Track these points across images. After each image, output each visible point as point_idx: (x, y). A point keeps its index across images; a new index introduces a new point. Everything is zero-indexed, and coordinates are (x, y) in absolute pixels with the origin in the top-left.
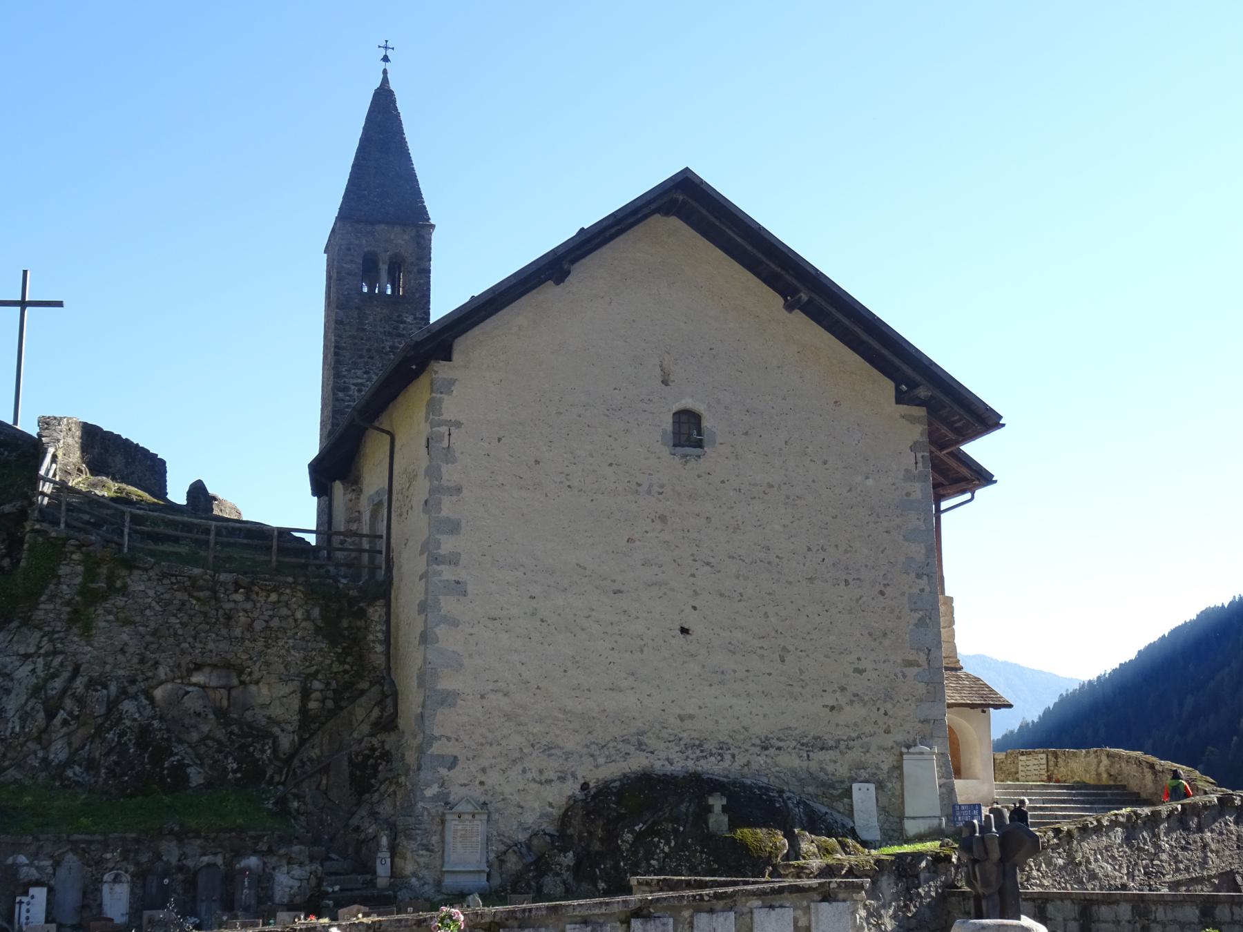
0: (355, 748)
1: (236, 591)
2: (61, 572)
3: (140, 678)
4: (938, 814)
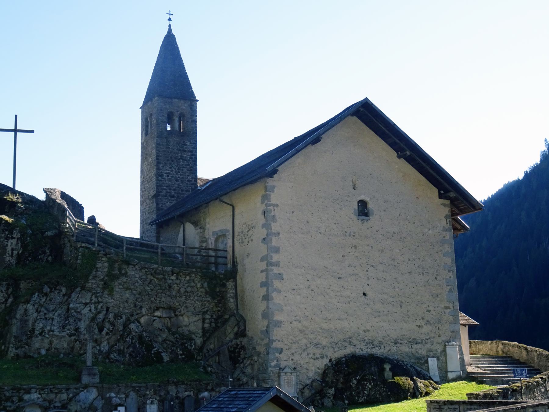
0: (230, 344)
1: (172, 275)
2: (97, 266)
4: (459, 370)
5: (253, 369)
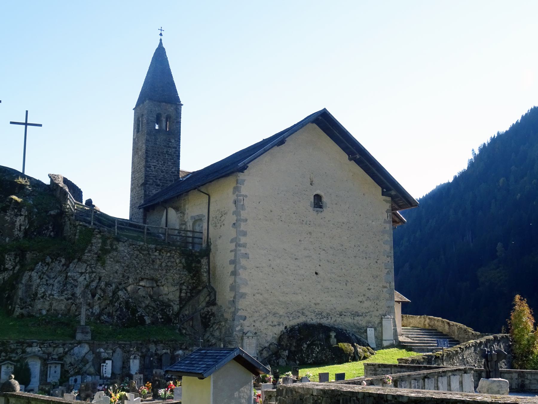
0: (202, 311)
1: (156, 251)
2: (92, 242)
3: (123, 283)
5: (221, 332)
